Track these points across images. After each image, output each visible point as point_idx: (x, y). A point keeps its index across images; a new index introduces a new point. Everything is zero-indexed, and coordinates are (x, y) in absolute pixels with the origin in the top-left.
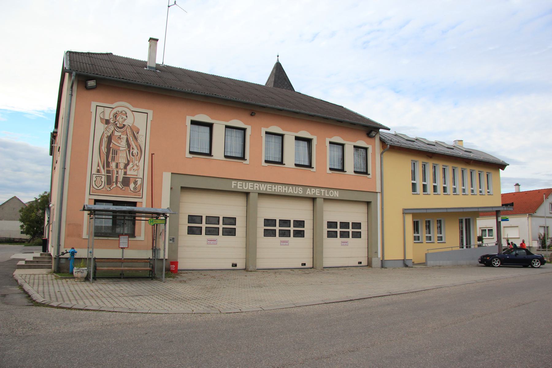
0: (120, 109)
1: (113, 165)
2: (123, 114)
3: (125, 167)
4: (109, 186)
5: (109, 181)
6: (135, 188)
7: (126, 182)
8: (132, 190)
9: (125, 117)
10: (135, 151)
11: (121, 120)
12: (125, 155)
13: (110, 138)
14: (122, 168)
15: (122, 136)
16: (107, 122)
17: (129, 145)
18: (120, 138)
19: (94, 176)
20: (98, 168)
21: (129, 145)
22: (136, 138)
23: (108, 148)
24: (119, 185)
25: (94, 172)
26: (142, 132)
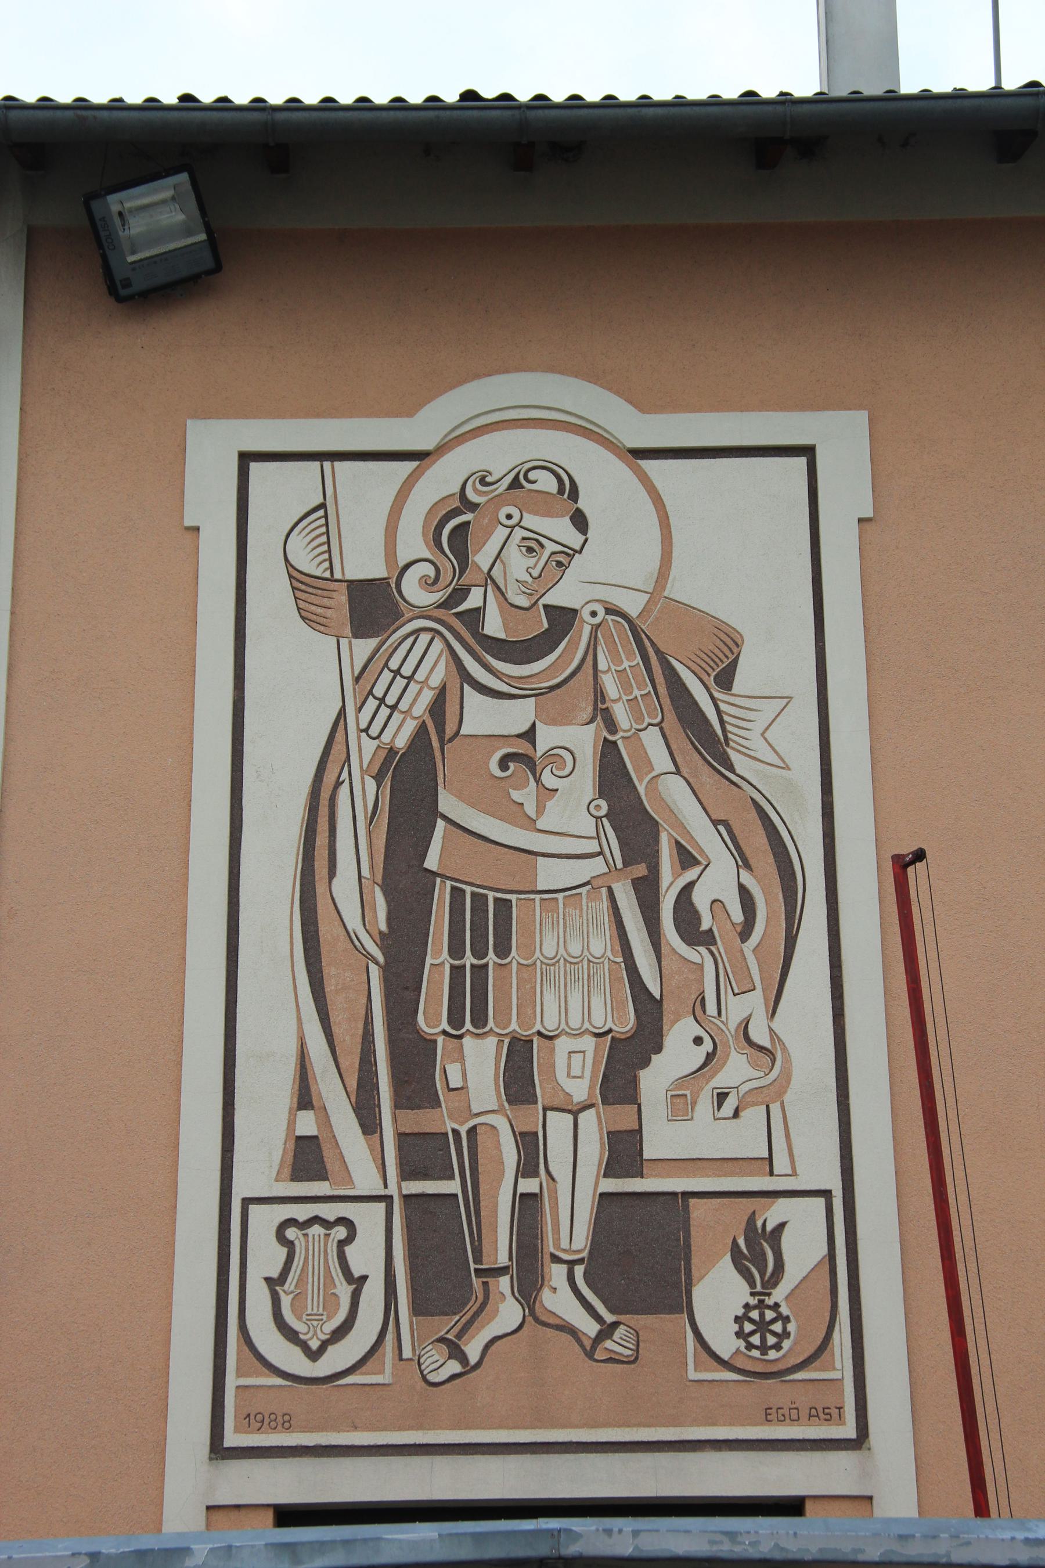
0: (499, 455)
1: (474, 1068)
2: (542, 504)
3: (619, 1081)
4: (446, 1325)
5: (441, 1265)
6: (758, 1323)
7: (642, 1253)
8: (726, 1344)
9: (562, 529)
10: (717, 883)
11: (518, 566)
12: (601, 944)
13: (412, 782)
14: (579, 1090)
15: (547, 737)
16: (372, 607)
17: (631, 822)
18: (523, 756)
19: (264, 1221)
20: (307, 1124)
21: (631, 822)
22: (707, 742)
23: (405, 880)
24: (559, 1299)
25: (259, 1169)
26: (773, 661)
